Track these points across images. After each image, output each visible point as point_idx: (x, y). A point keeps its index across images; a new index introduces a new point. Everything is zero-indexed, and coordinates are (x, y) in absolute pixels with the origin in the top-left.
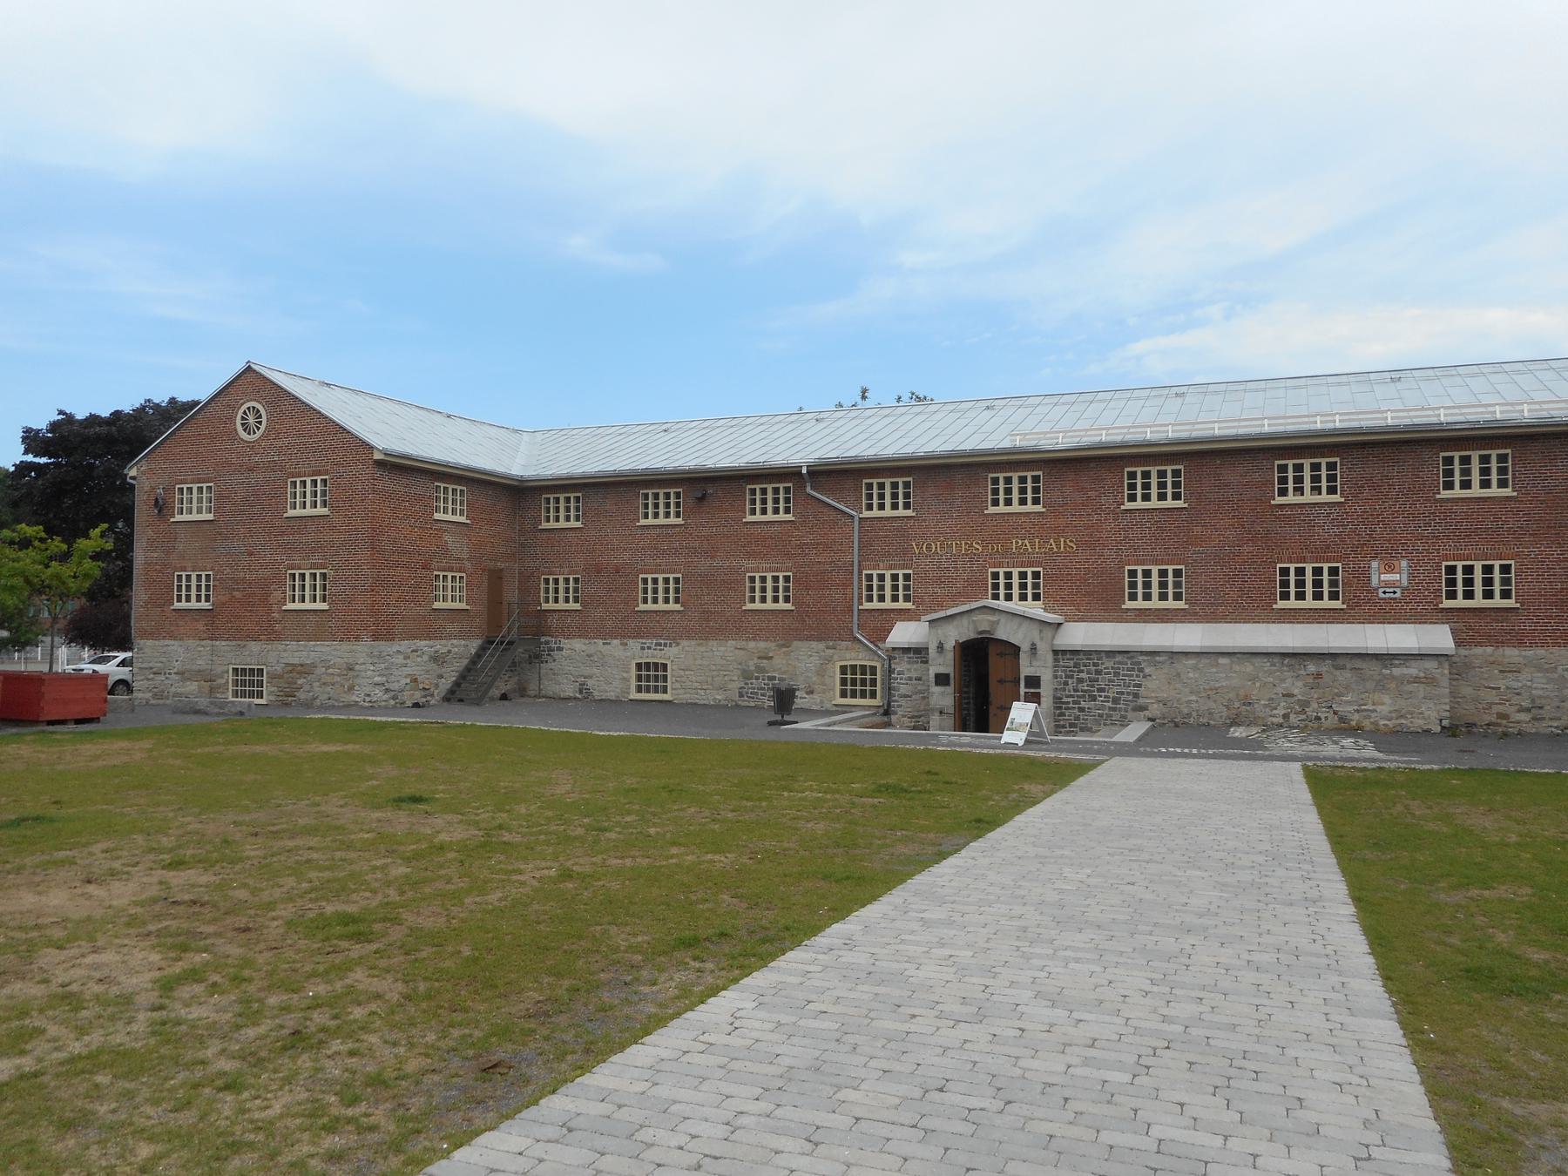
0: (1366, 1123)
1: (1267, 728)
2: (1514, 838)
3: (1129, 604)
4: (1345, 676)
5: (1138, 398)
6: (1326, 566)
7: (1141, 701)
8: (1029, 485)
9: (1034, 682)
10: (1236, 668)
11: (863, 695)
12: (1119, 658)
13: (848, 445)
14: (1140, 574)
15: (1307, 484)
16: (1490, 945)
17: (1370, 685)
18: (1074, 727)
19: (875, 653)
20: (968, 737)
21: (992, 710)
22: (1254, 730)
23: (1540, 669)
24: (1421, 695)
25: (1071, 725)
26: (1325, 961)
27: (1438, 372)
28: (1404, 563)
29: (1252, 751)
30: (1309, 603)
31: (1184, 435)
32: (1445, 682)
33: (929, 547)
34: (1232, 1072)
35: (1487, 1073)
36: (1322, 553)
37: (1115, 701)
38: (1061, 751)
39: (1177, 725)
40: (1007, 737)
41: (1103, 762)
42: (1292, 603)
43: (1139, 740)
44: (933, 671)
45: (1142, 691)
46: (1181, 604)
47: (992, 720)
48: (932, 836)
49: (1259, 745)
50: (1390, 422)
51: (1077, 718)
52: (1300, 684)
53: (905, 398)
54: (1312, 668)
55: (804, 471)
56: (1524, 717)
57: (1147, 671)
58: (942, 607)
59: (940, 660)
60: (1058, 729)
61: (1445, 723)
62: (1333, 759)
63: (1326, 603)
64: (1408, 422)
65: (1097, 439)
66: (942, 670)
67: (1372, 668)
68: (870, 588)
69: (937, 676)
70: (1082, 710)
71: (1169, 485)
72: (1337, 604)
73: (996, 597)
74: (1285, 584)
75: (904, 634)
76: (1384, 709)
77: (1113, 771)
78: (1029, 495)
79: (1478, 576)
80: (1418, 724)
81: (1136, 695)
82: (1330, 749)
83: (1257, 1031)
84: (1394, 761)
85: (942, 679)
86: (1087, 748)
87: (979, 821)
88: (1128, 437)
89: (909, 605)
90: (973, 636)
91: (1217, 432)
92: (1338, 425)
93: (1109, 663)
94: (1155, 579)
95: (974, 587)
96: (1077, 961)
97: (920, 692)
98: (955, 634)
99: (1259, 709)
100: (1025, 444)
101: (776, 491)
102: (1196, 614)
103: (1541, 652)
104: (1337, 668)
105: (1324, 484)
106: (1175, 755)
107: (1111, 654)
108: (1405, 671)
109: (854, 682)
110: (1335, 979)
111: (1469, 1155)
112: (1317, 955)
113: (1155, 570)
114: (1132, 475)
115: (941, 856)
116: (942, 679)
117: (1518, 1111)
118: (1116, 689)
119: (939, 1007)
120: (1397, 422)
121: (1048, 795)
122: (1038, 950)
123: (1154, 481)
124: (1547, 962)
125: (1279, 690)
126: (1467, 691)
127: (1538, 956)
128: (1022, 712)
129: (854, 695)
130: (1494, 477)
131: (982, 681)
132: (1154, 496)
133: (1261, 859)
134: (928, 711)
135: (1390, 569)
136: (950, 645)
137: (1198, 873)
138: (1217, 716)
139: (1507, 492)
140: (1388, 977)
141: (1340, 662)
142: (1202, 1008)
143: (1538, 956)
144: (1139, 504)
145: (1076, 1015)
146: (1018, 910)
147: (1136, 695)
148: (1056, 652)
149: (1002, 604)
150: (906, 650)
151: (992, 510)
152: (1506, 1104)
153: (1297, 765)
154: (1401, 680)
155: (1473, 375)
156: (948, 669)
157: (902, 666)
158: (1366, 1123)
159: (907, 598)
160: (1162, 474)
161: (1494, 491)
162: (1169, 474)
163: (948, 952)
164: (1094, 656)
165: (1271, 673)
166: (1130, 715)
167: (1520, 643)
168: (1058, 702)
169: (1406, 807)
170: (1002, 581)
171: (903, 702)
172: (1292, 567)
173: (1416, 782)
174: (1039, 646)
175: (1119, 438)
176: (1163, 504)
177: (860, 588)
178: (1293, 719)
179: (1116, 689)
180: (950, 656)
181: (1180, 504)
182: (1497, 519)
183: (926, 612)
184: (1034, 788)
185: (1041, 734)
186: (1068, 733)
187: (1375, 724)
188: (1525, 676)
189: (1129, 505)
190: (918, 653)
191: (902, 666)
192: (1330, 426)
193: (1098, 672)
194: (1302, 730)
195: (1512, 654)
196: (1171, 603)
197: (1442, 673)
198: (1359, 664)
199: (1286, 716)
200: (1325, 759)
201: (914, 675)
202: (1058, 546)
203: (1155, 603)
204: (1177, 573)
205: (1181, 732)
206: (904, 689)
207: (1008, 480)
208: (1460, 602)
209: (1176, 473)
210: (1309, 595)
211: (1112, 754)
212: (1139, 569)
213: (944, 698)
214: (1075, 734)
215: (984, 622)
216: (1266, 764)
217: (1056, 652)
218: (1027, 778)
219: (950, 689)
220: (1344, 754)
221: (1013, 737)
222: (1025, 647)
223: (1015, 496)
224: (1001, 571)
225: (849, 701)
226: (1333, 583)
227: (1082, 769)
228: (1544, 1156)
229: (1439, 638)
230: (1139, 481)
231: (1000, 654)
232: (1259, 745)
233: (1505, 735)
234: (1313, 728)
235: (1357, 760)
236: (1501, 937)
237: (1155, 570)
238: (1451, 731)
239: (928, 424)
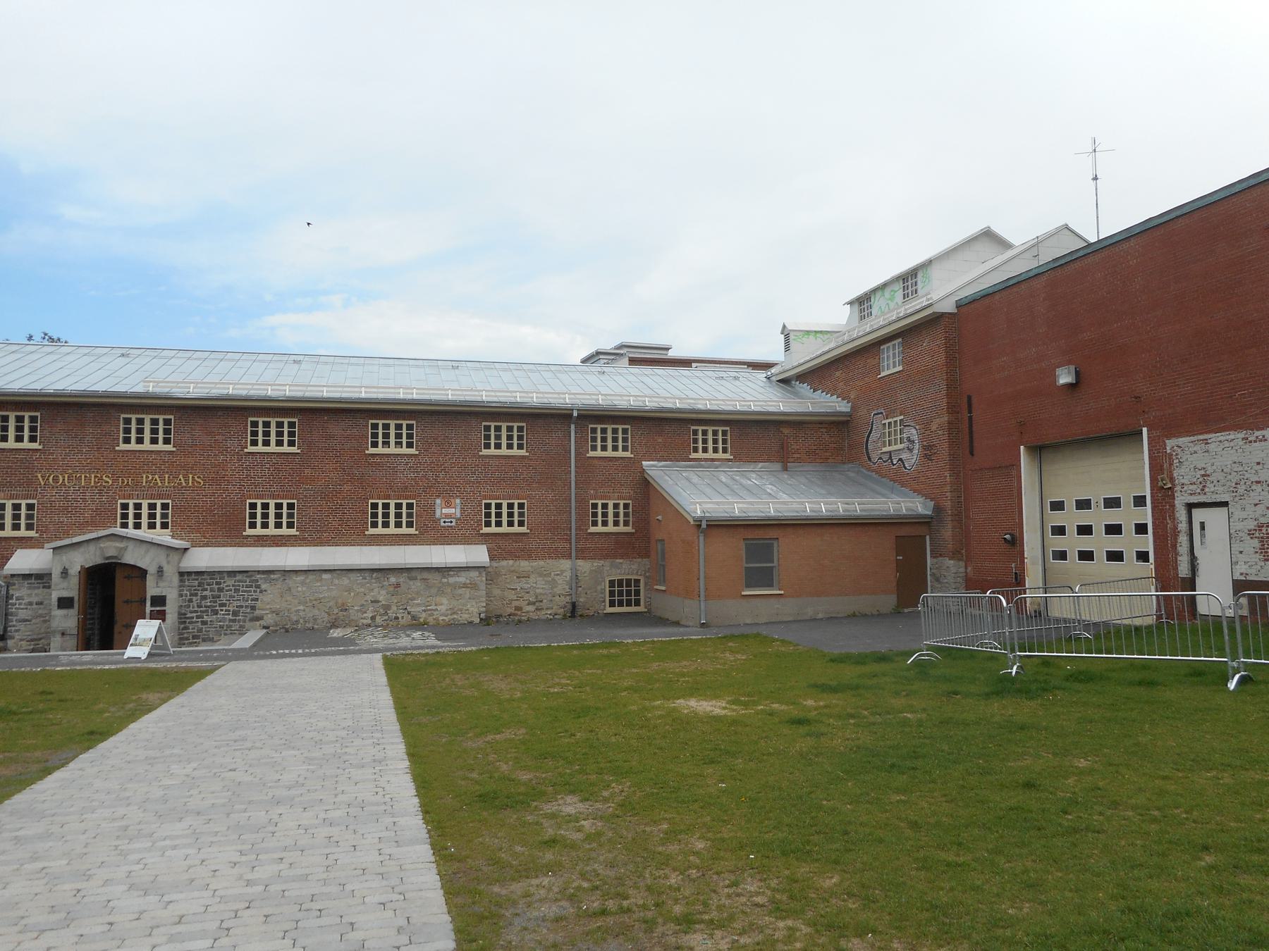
0: (400, 930)
1: (359, 628)
2: (519, 695)
3: (249, 532)
4: (417, 585)
5: (263, 361)
6: (404, 502)
7: (257, 613)
8: (515, 434)
9: (159, 601)
10: (336, 581)
11: (629, 604)
12: (239, 577)
13: (9, 378)
14: (259, 506)
15: (392, 440)
16: (496, 775)
17: (434, 591)
18: (197, 638)
20: (89, 655)
21: (117, 628)
22: (349, 630)
23: (541, 575)
24: (468, 596)
25: (194, 637)
26: (384, 807)
27: (482, 365)
28: (458, 501)
29: (346, 647)
30: (392, 530)
31: (299, 394)
32: (483, 587)
33: (56, 479)
34: (300, 915)
35: (485, 869)
36: (403, 492)
37: (235, 613)
38: (183, 660)
39: (287, 631)
40: (130, 652)
41: (219, 667)
42: (380, 530)
43: (255, 645)
44: (55, 595)
45: (259, 604)
46: (293, 532)
47: (116, 636)
48: (38, 754)
49: (352, 642)
50: (450, 397)
51: (200, 630)
52: (383, 592)
53: (37, 337)
54: (393, 580)
55: (575, 414)
56: (531, 608)
57: (263, 587)
58: (67, 534)
59: (65, 585)
60: (181, 641)
61: (483, 616)
62: (405, 649)
63: (404, 530)
64: (462, 398)
65: (225, 392)
66: (65, 594)
67: (434, 578)
70: (204, 623)
71: (286, 434)
72: (412, 531)
73: (125, 525)
74: (375, 515)
75: (24, 561)
76: (443, 608)
77: (230, 676)
78: (515, 442)
79: (145, 511)
80: (464, 617)
81: (253, 608)
82: (404, 641)
83: (325, 876)
84: (447, 646)
85: (65, 603)
86: (207, 656)
87: (92, 733)
88: (252, 393)
89: (32, 533)
90: (99, 561)
91: (325, 395)
92: (415, 397)
94: (272, 511)
95: (103, 516)
96: (174, 847)
97: (41, 616)
98: (80, 560)
99: (353, 614)
100: (158, 390)
101: (510, 429)
102: (304, 539)
103: (541, 563)
104: (411, 579)
105: (404, 440)
106: (284, 656)
107: (232, 573)
108: (457, 579)
109: (620, 593)
110: (388, 820)
111: (469, 934)
112: (377, 804)
113: (272, 503)
114: (255, 424)
115: (47, 771)
116: (65, 603)
117: (504, 892)
118: (235, 604)
119: (24, 922)
120: (455, 398)
121: (164, 701)
122: (137, 846)
123: (273, 430)
124: (531, 780)
125: (369, 598)
126: (497, 592)
127: (525, 776)
128: (146, 629)
129: (621, 604)
130: (26, 433)
131: (107, 601)
132: (273, 442)
133: (343, 733)
134: (49, 634)
135: (448, 505)
136: (75, 570)
137: (292, 752)
138: (319, 621)
139: (523, 452)
140: (426, 810)
141: (414, 574)
142: (282, 866)
143: (525, 776)
144: (260, 448)
145: (166, 898)
146: (121, 811)
147: (253, 608)
148: (181, 574)
149: (131, 532)
150: (26, 577)
151: (123, 447)
152: (496, 889)
153: (378, 657)
154: (455, 586)
155: (505, 370)
157: (21, 592)
158: (400, 930)
160: (155, 422)
161: (515, 452)
162: (286, 425)
163: (39, 865)
164: (217, 576)
165: (362, 585)
166: (248, 624)
167: (529, 557)
168: (182, 618)
169: (453, 680)
170: (131, 511)
171: (22, 627)
172: (380, 502)
173: (461, 661)
174: (166, 568)
175: (244, 393)
176: (280, 450)
178: (379, 620)
179: (235, 604)
181: (294, 449)
182: (517, 471)
183: (50, 540)
184: (152, 697)
185: (165, 647)
186: (191, 644)
187: (436, 619)
188: (532, 580)
189: (251, 449)
190: (40, 579)
191: (21, 592)
192: (409, 397)
193: (220, 590)
194: (385, 628)
195: (524, 565)
196: (284, 531)
197: (481, 579)
198: (425, 575)
199: (373, 618)
200: (400, 649)
201: (35, 600)
202: (187, 481)
203: (272, 531)
204: (291, 506)
205: (291, 636)
206: (23, 614)
207: (498, 429)
208: (493, 529)
209: (291, 425)
210: (392, 524)
211: (229, 660)
212: (493, 502)
213: (68, 620)
214: (197, 644)
215: (111, 549)
216: (356, 657)
217: (181, 574)
218: (146, 688)
219: (73, 612)
220: (414, 644)
221: (136, 651)
222: (152, 570)
223: (610, 443)
224: (131, 503)
226: (409, 515)
227: (201, 674)
228: (517, 921)
229: (479, 554)
230: (260, 429)
232: (352, 642)
233: (520, 621)
234: (393, 626)
235: (422, 648)
236: (504, 767)
237: (272, 503)
238: (486, 621)
239: (59, 364)
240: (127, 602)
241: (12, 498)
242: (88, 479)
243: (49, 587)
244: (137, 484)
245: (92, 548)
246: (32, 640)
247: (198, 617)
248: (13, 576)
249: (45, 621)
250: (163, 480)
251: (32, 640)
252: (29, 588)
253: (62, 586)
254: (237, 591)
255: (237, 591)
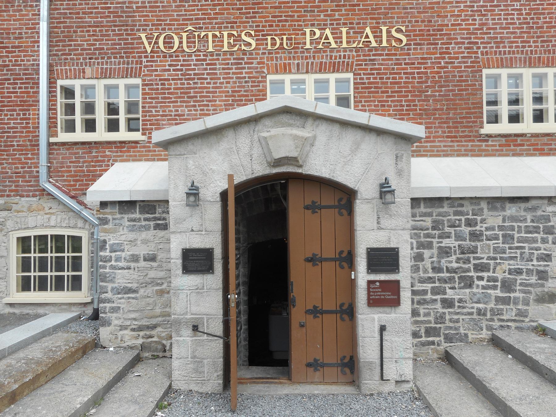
3: (489, 129)
11: (59, 285)
12: (511, 210)
19: (78, 215)
33: (168, 42)
37: (507, 286)
44: (177, 244)
51: (440, 319)
59: (194, 222)
66: (197, 242)
68: (70, 109)
69: (396, 303)
70: (448, 303)
81: (543, 275)
85: (196, 261)
90: (259, 169)
93: (493, 219)
97: (153, 282)
98: (227, 165)
107: (497, 202)
116: (196, 261)
118: (506, 265)
129: (42, 285)
136: (215, 186)
147: (543, 275)
150: (127, 206)
156: (212, 240)
157: (123, 235)
159: (131, 127)
164: (468, 208)
171: (121, 302)
177: (52, 108)
179: (506, 265)
180: (213, 213)
190: (151, 209)
193: (475, 236)
201: (142, 250)
202: (378, 38)
206: (122, 278)
213: (203, 299)
215: (284, 141)
222: (367, 190)
225: (34, 296)
231: (313, 208)
240: (312, 260)
241: (104, 75)
242: (219, 41)
243: (165, 227)
244: (297, 46)
245: (244, 139)
246: (140, 329)
247: (435, 291)
248: (104, 204)
249: (161, 293)
250: (338, 38)
251: (140, 329)
252: (132, 229)
253: (187, 225)
254: (508, 238)
255: (508, 238)
